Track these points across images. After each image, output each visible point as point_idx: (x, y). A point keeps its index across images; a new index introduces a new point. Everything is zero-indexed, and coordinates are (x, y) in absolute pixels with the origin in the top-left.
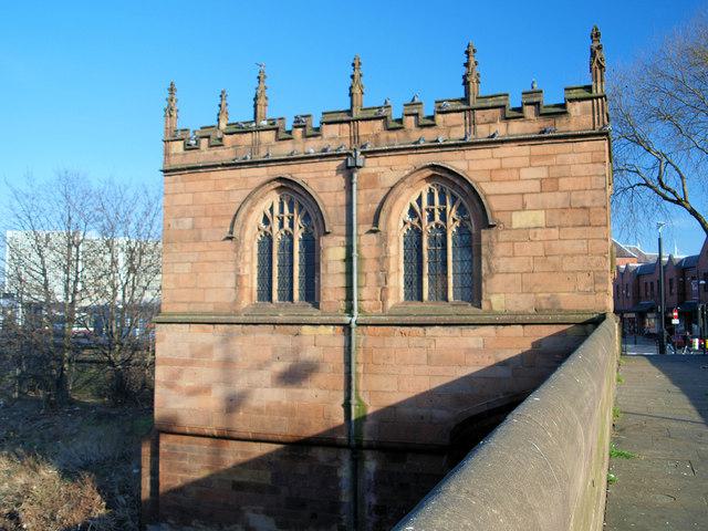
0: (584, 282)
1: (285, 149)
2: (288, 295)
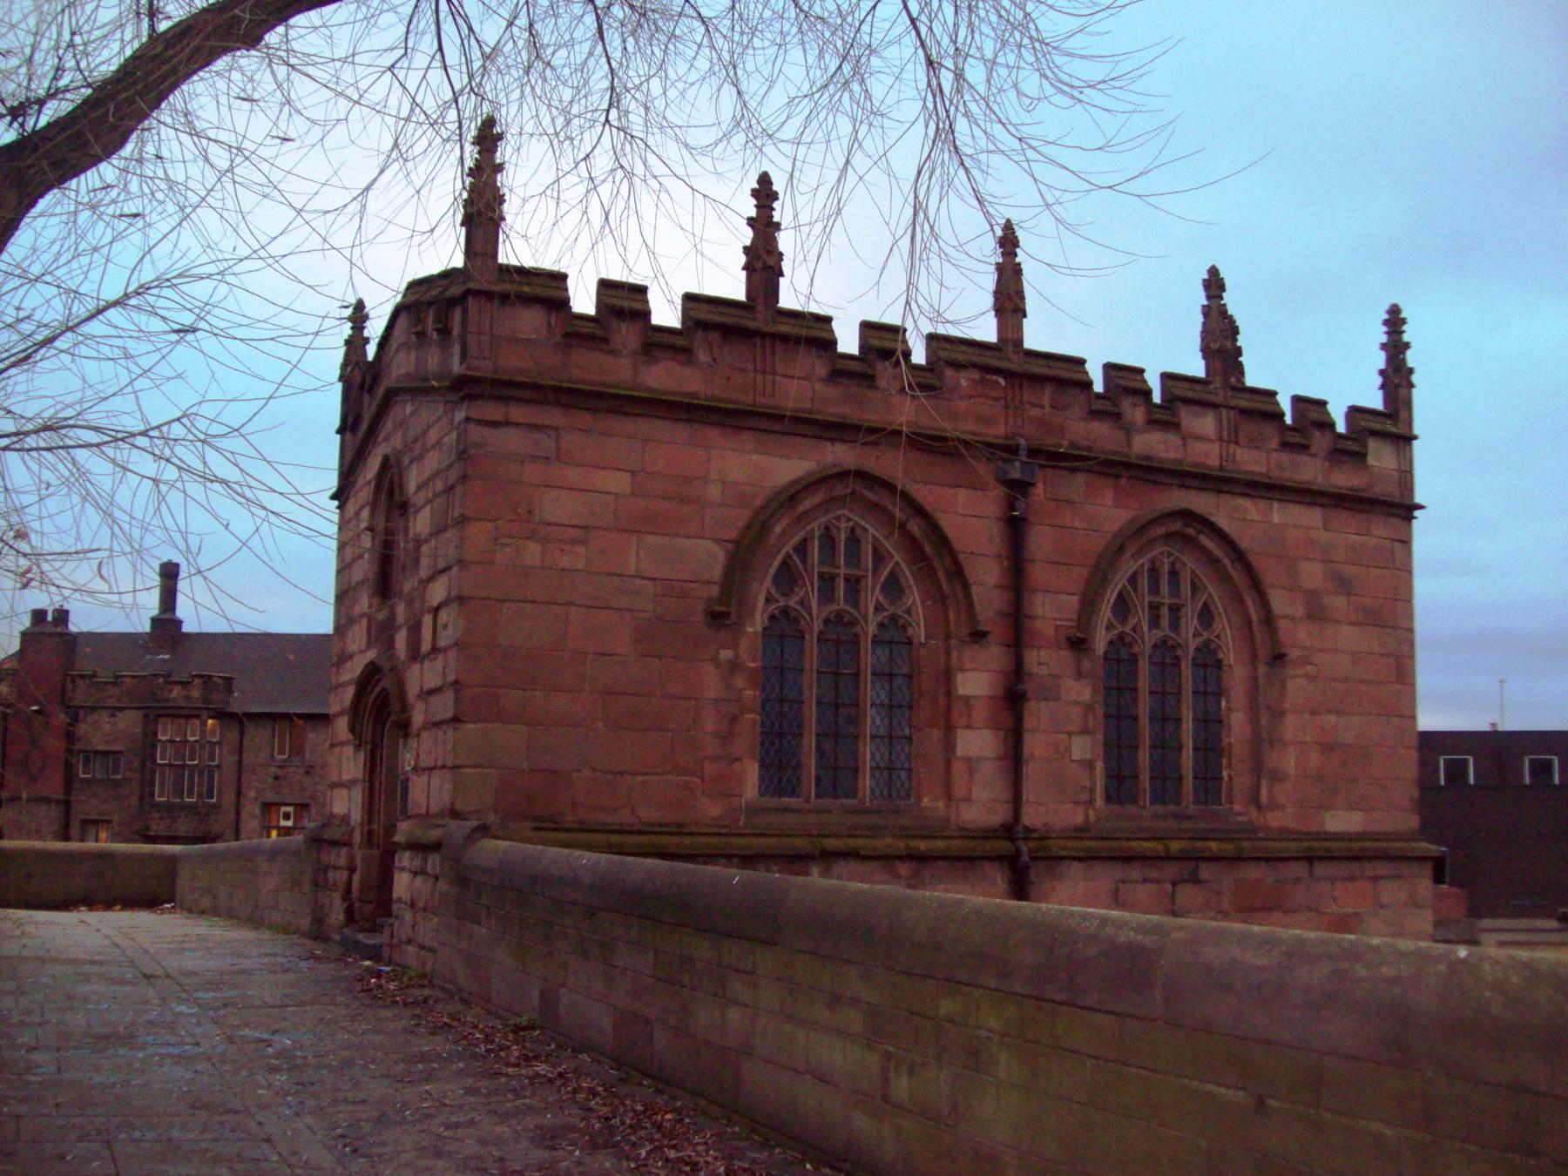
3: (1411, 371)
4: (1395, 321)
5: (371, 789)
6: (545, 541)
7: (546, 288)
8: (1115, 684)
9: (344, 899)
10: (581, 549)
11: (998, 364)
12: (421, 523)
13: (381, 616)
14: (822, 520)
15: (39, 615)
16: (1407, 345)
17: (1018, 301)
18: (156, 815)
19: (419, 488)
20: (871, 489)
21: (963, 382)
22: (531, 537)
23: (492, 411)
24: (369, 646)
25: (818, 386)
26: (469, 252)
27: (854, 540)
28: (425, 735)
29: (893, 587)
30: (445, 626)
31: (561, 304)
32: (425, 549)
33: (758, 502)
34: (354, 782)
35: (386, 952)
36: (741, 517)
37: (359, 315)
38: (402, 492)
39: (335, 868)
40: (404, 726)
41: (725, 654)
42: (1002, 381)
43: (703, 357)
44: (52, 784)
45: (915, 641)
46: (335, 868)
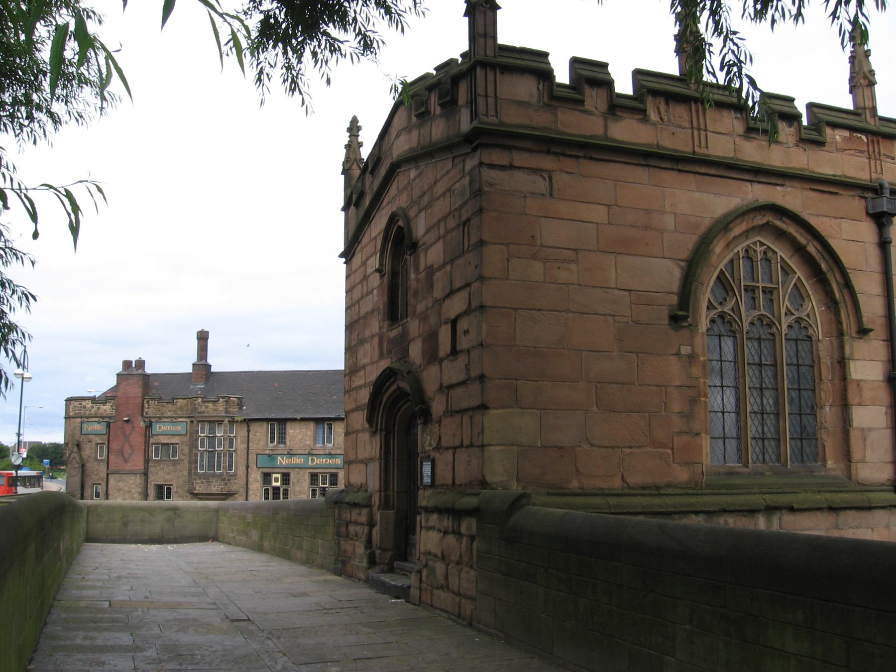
5: (387, 464)
6: (545, 260)
7: (533, 64)
8: (796, 386)
9: (366, 548)
10: (573, 267)
11: (858, 124)
12: (433, 255)
13: (393, 334)
14: (744, 245)
15: (127, 364)
17: (871, 78)
18: (198, 481)
19: (428, 231)
20: (781, 220)
21: (838, 137)
22: (534, 257)
23: (498, 157)
24: (381, 356)
25: (737, 139)
28: (446, 421)
29: (799, 295)
30: (466, 332)
31: (547, 75)
32: (438, 275)
33: (702, 229)
34: (372, 459)
35: (414, 592)
36: (690, 241)
37: (354, 128)
38: (411, 237)
39: (356, 523)
40: (426, 414)
41: (685, 350)
42: (864, 138)
43: (653, 116)
44: (137, 462)
45: (814, 339)
46: (356, 523)
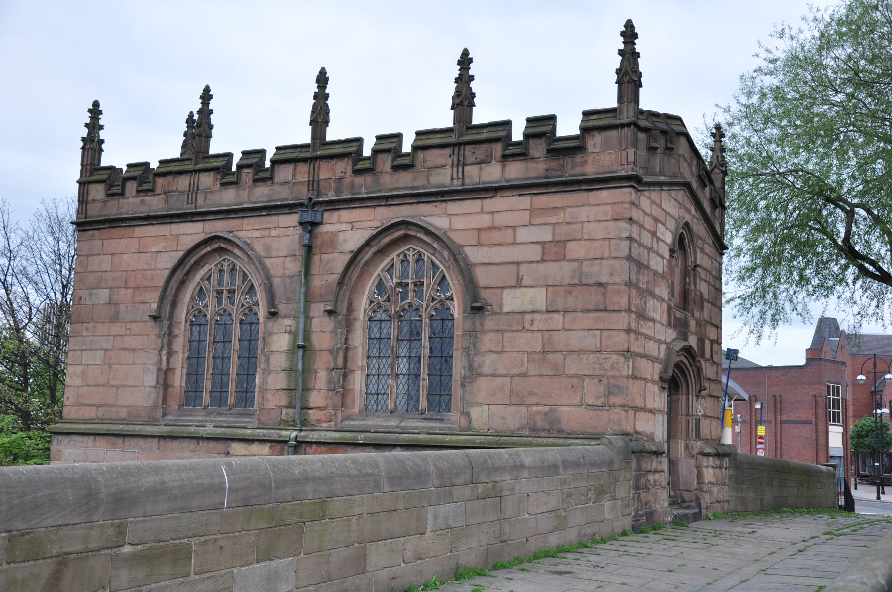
0: (593, 392)
1: (229, 198)
2: (219, 399)
3: (102, 141)
4: (630, 34)
16: (211, 112)
26: (313, 137)
27: (419, 260)
